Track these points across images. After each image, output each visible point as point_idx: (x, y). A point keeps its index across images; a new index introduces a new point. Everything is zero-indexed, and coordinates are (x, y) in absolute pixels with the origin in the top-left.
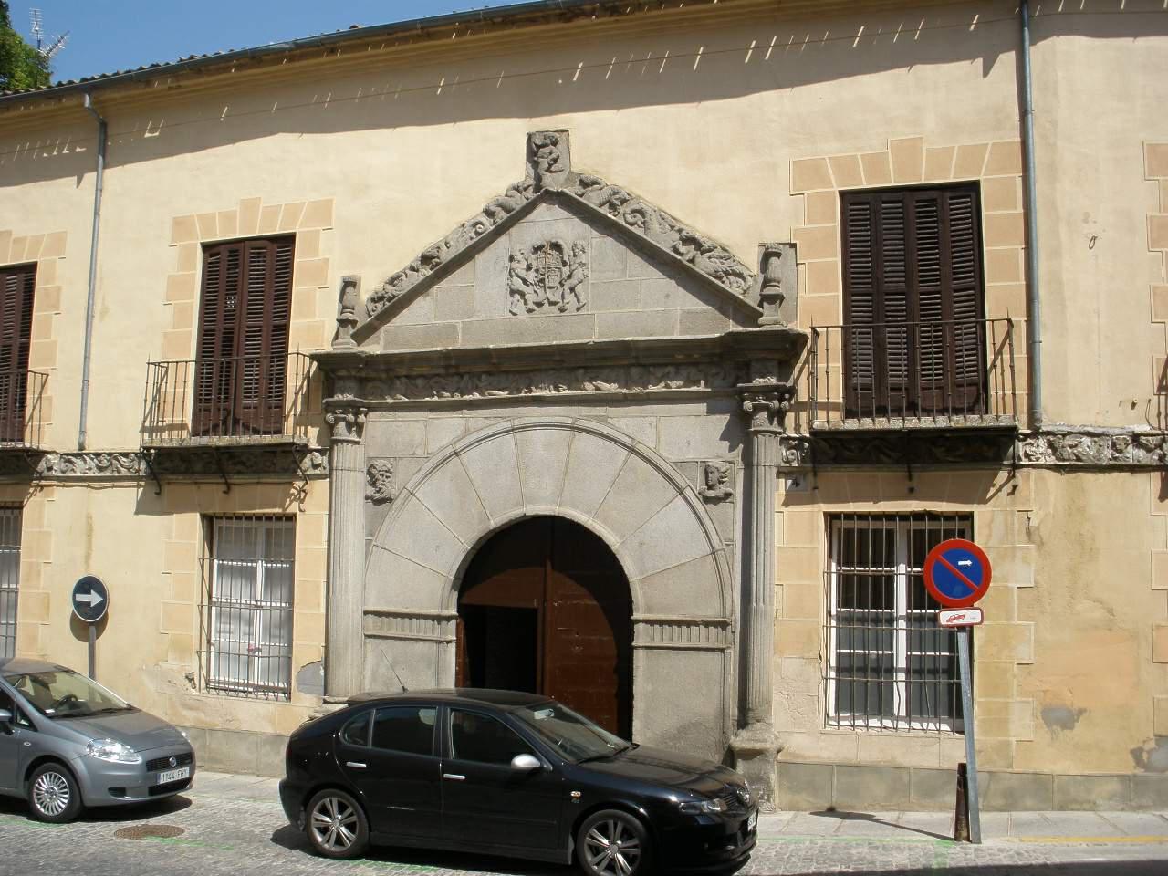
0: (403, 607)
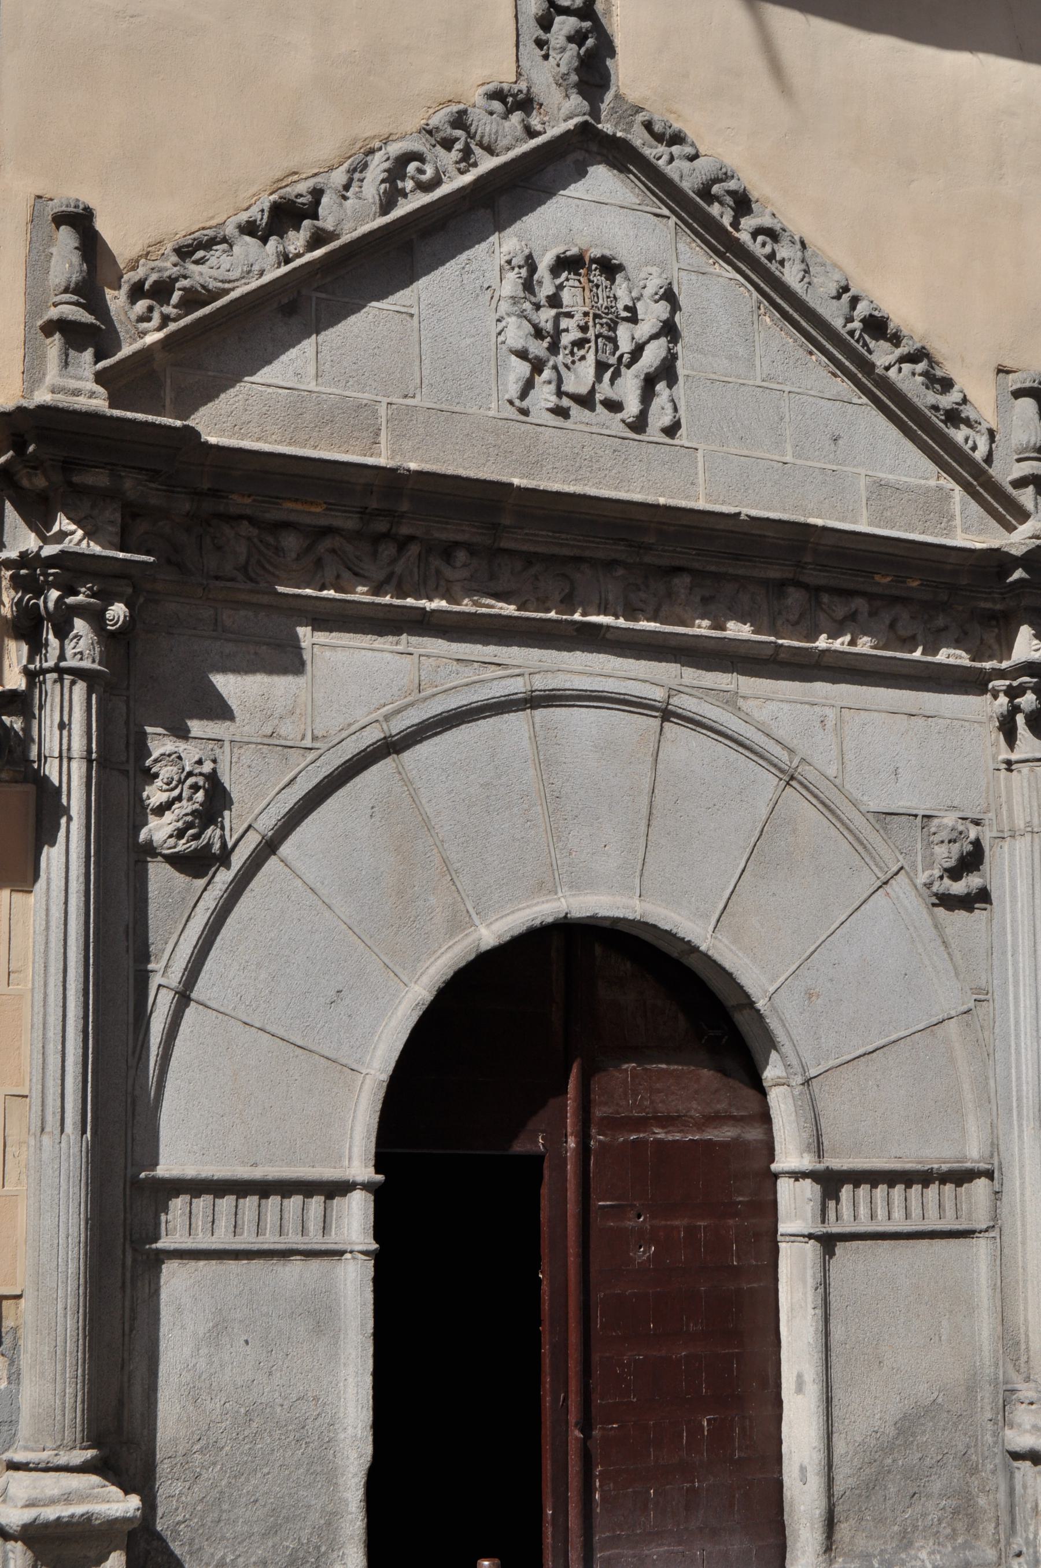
0: (243, 1163)
